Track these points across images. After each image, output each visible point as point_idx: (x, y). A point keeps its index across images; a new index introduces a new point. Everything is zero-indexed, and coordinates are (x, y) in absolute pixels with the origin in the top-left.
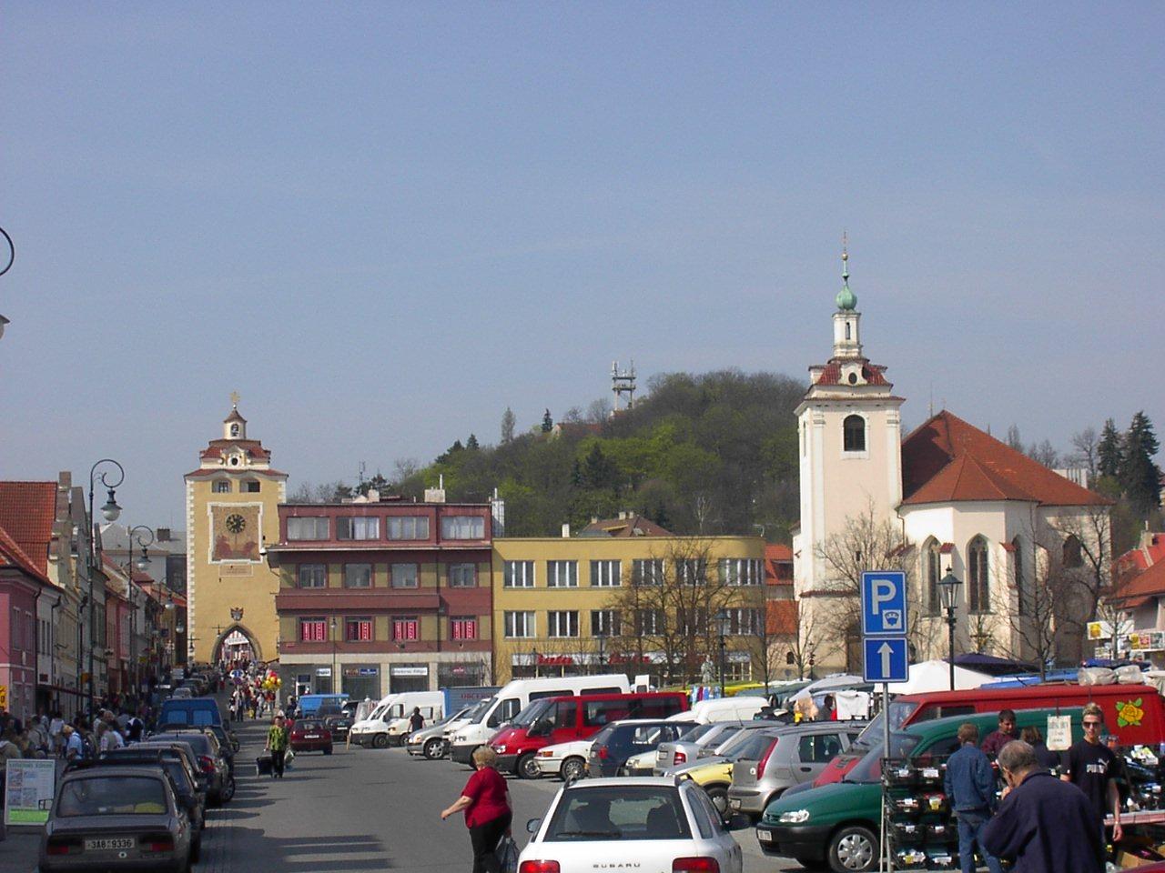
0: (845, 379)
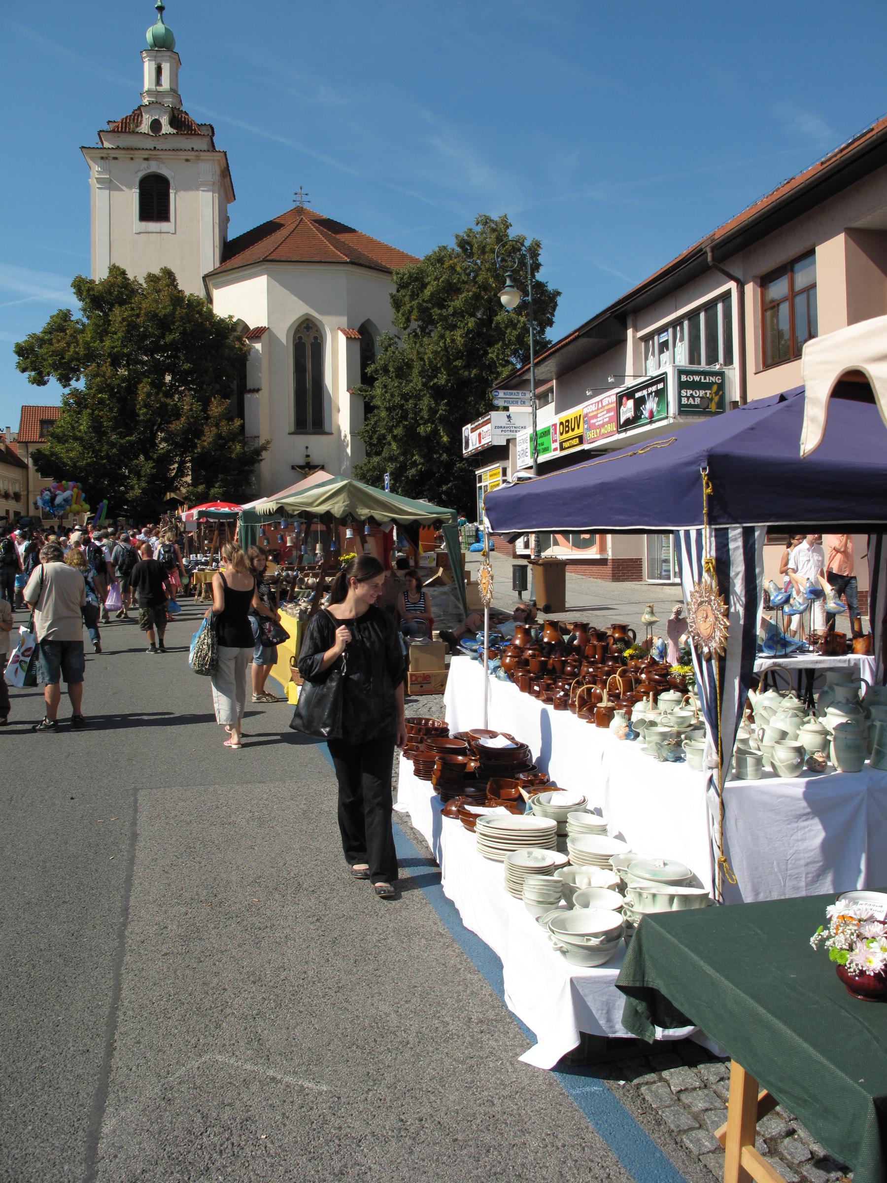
0: (145, 127)
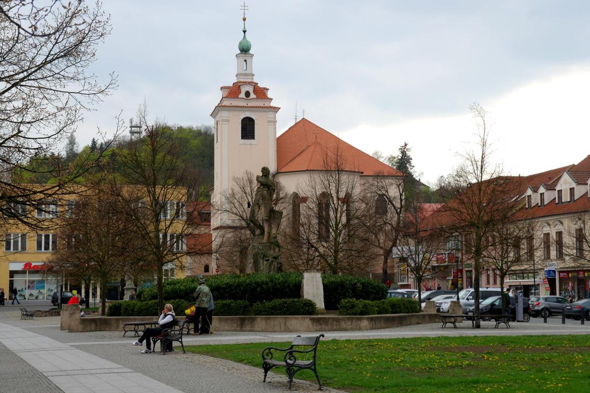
0: (242, 95)
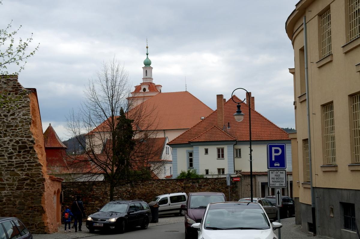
0: (142, 91)
